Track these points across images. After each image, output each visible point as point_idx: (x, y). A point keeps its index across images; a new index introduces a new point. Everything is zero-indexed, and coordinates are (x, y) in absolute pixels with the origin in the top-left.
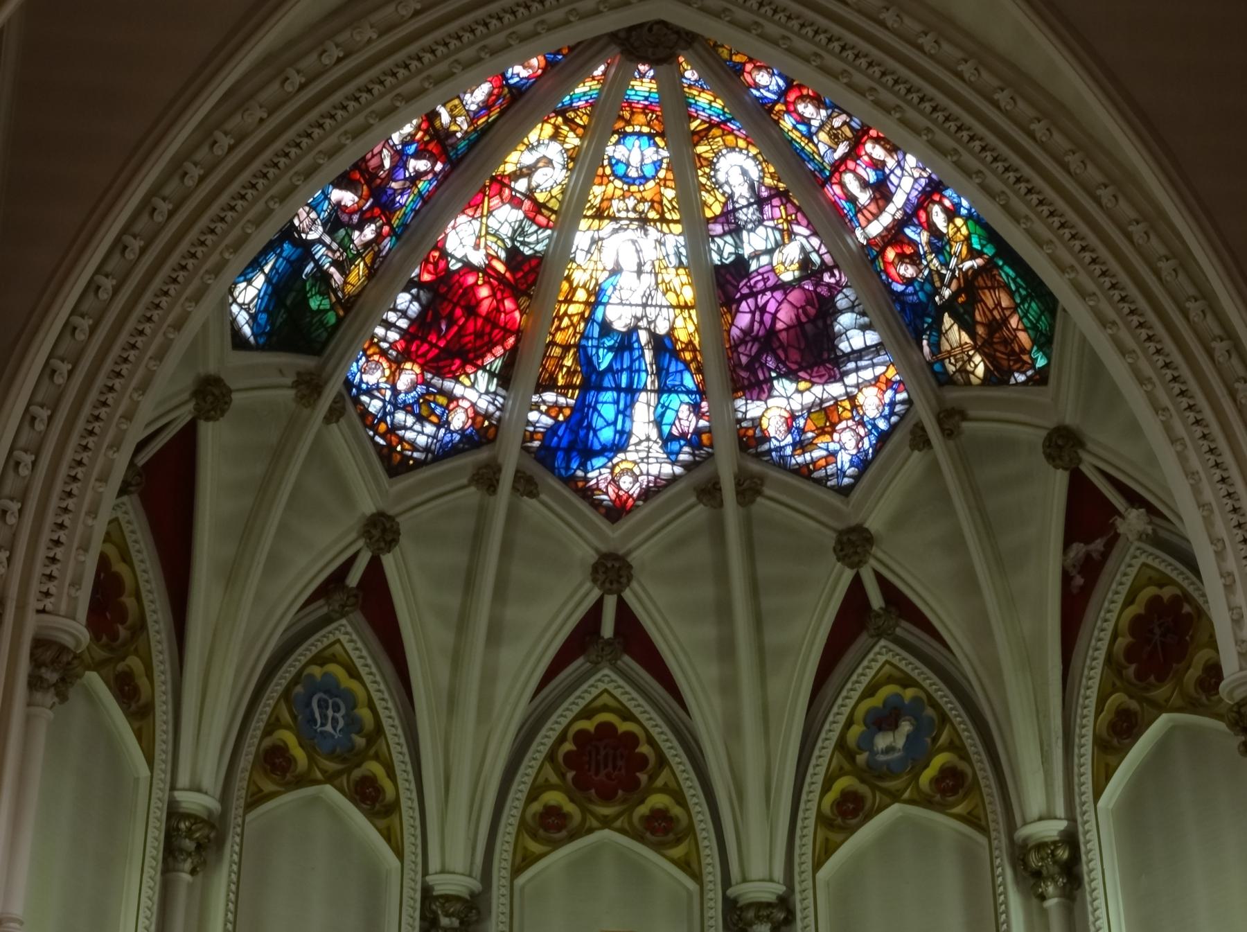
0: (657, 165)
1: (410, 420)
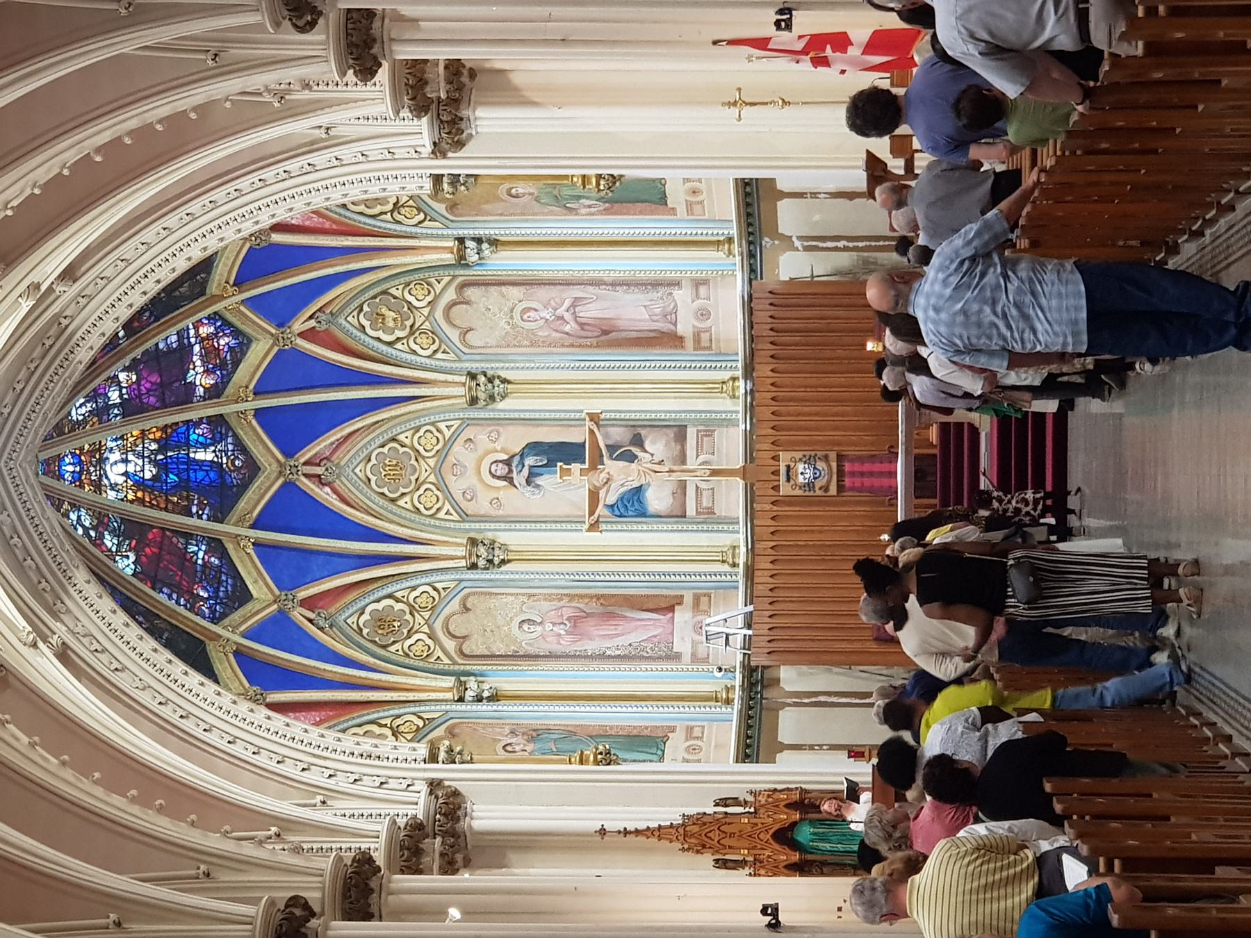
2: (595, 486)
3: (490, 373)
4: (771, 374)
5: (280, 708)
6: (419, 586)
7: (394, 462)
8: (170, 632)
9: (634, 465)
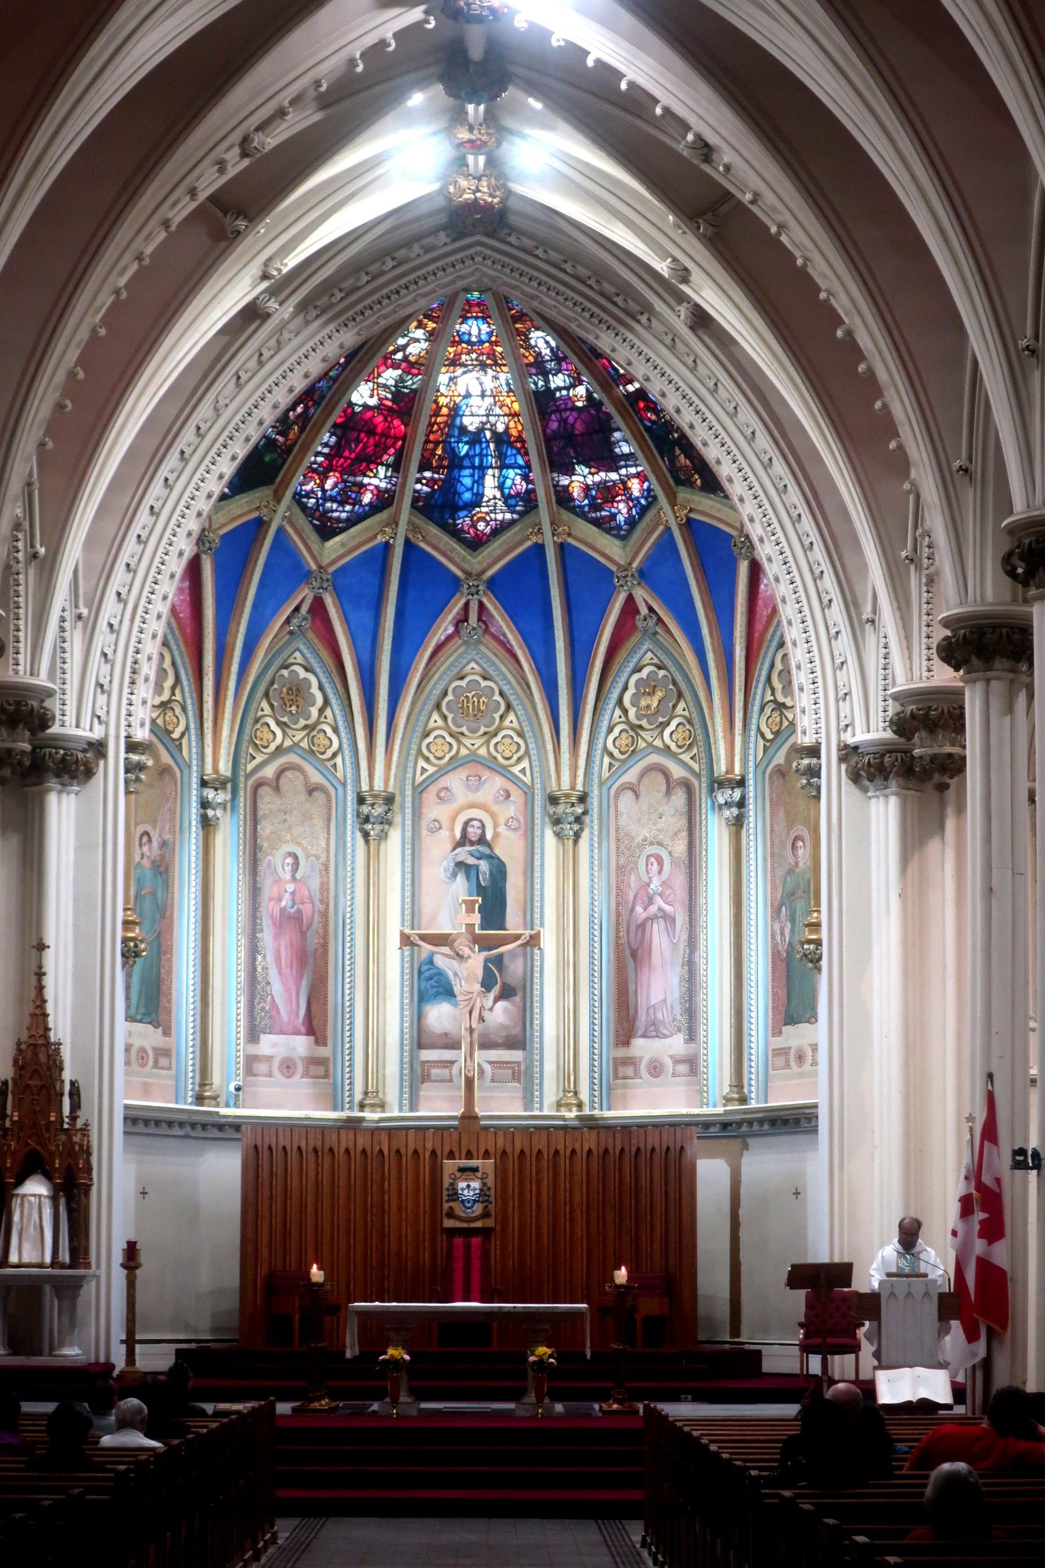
0: (490, 334)
1: (335, 506)
2: (455, 941)
3: (587, 819)
4: (586, 1149)
5: (194, 569)
6: (339, 736)
7: (482, 708)
8: (284, 444)
9: (477, 987)
